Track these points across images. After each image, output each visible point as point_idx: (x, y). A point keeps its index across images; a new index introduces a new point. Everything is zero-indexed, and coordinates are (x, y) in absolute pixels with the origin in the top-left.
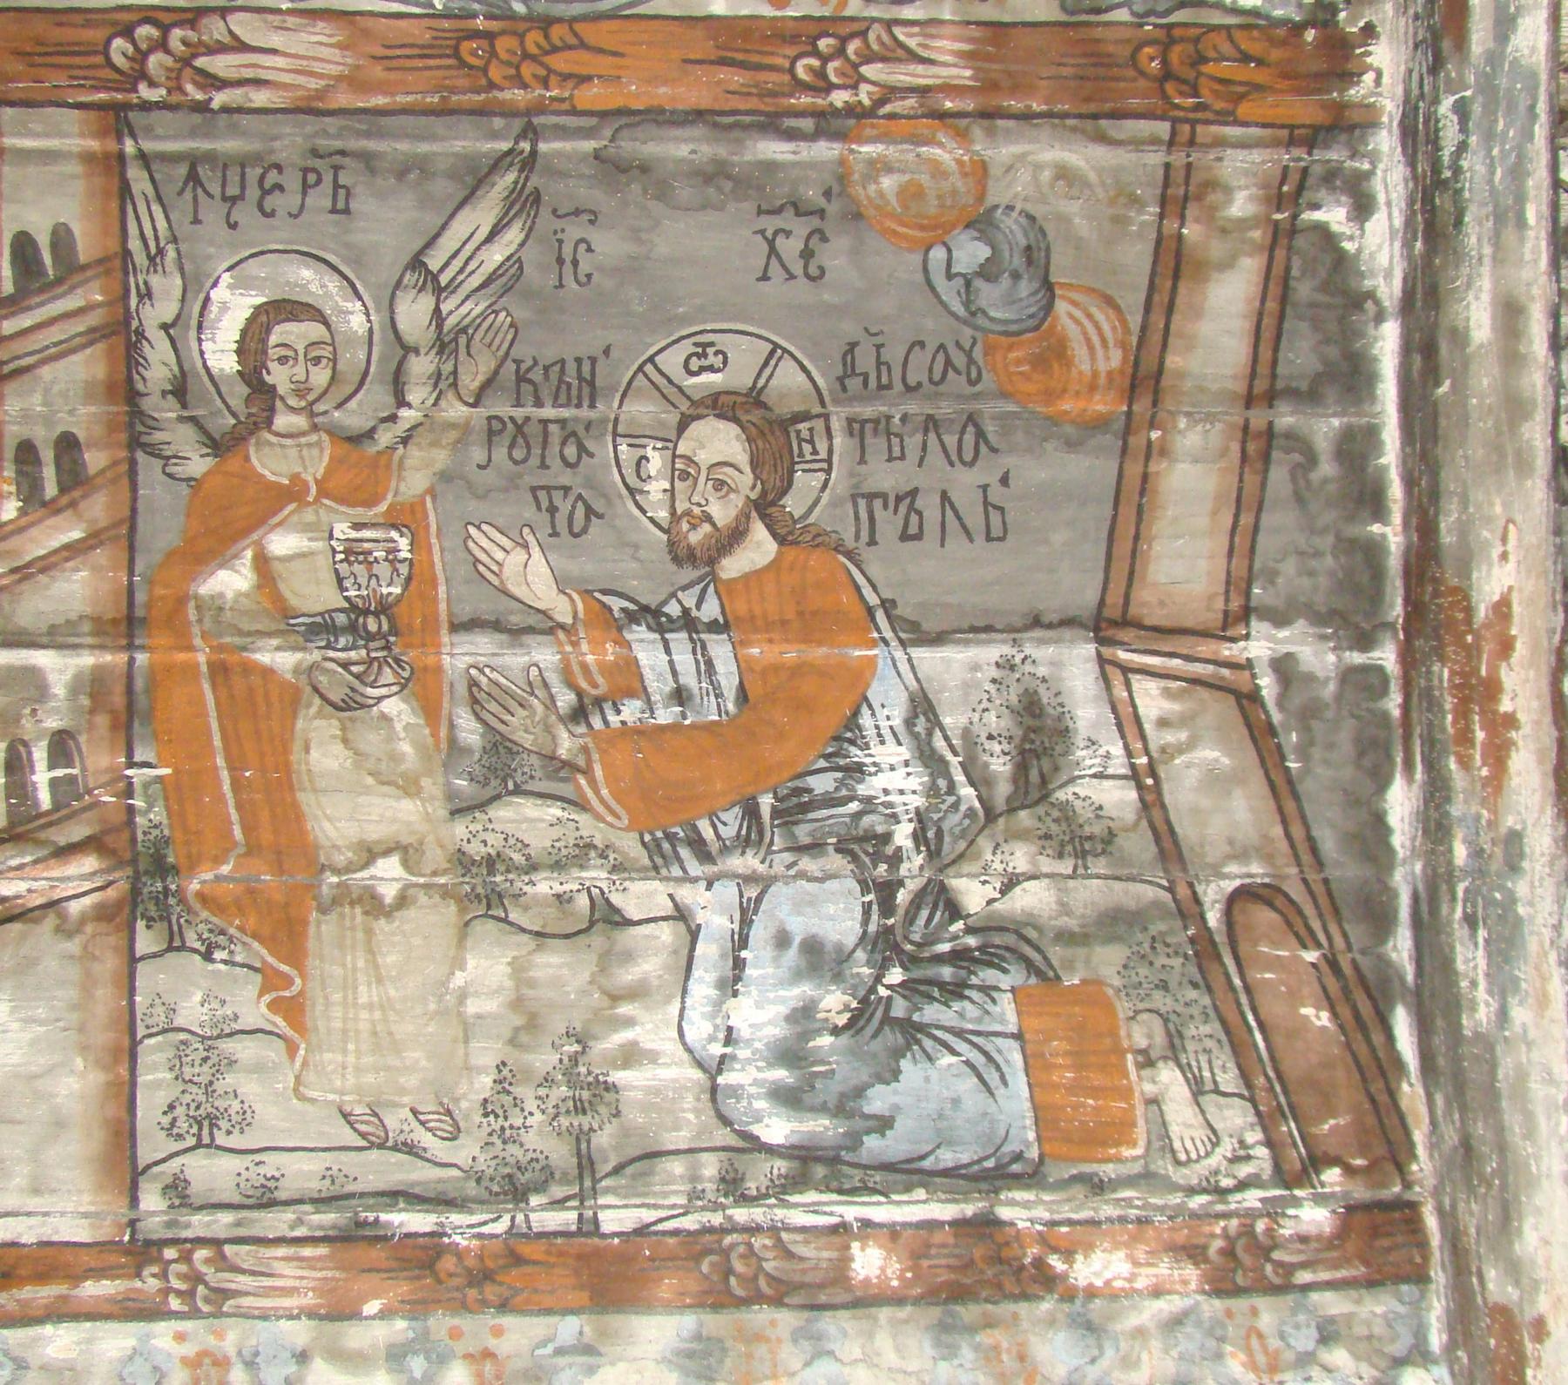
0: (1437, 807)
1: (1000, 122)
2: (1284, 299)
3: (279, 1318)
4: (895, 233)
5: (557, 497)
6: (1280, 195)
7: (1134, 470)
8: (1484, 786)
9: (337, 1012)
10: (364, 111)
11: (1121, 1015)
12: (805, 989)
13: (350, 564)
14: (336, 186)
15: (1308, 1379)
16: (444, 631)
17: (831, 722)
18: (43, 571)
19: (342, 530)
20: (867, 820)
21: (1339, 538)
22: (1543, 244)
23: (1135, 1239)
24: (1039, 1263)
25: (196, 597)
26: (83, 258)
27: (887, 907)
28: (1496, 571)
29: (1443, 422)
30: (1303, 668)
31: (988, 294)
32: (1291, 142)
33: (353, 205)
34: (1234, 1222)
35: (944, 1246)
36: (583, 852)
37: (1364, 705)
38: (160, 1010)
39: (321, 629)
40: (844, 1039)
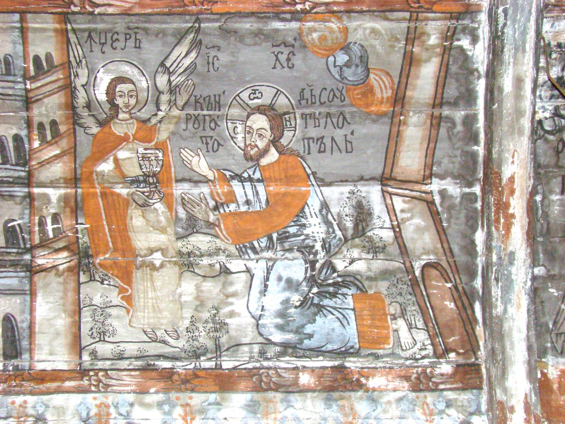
0: (490, 241)
1: (352, 14)
2: (447, 72)
3: (124, 393)
4: (317, 52)
5: (209, 139)
6: (447, 36)
7: (395, 129)
8: (503, 237)
9: (142, 300)
10: (144, 14)
11: (386, 303)
12: (287, 294)
13: (144, 161)
14: (136, 39)
15: (442, 418)
16: (174, 182)
17: (296, 211)
18: (47, 163)
19: (141, 150)
20: (307, 241)
21: (462, 151)
22: (531, 58)
23: (388, 373)
24: (358, 380)
25: (96, 171)
26: (56, 63)
27: (313, 269)
29: (495, 117)
30: (449, 193)
31: (348, 72)
32: (451, 18)
33: (141, 46)
34: (420, 369)
35: (328, 374)
36: (218, 251)
37: (469, 205)
38: (88, 299)
39: (135, 181)
40: (298, 310)
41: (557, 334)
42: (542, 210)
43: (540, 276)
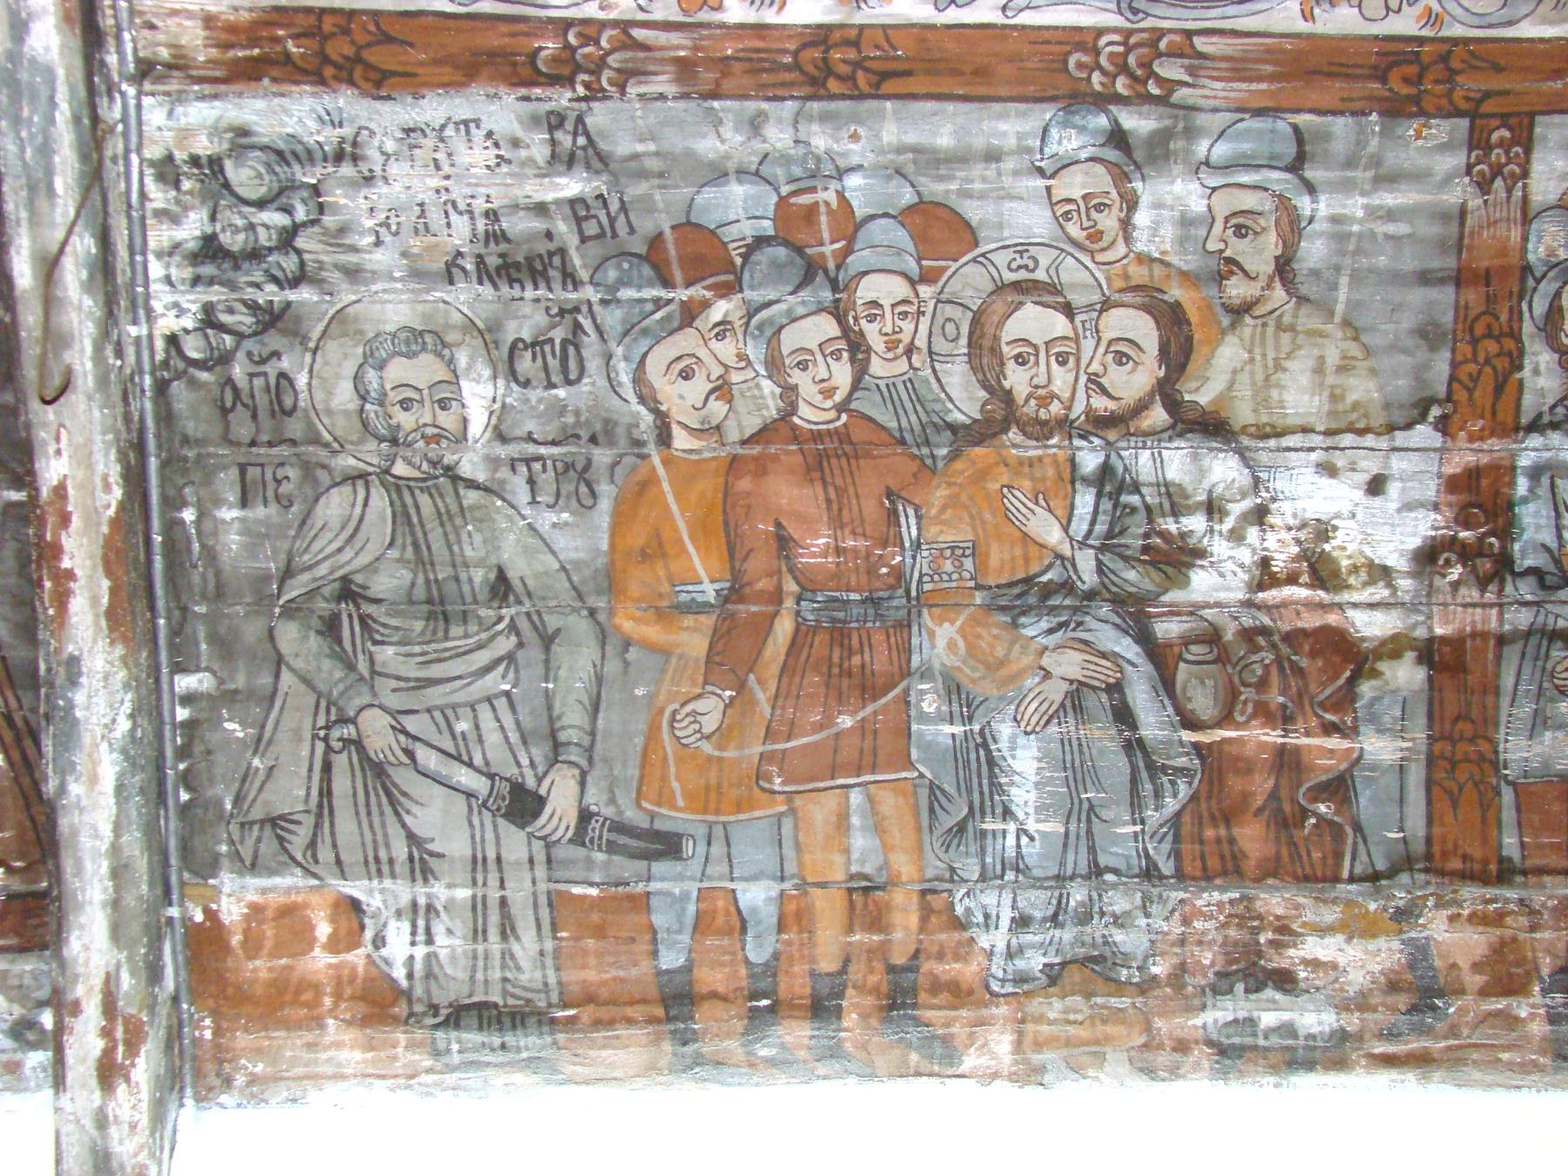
28: (53, 462)
41: (242, 825)
42: (200, 541)
43: (202, 694)
